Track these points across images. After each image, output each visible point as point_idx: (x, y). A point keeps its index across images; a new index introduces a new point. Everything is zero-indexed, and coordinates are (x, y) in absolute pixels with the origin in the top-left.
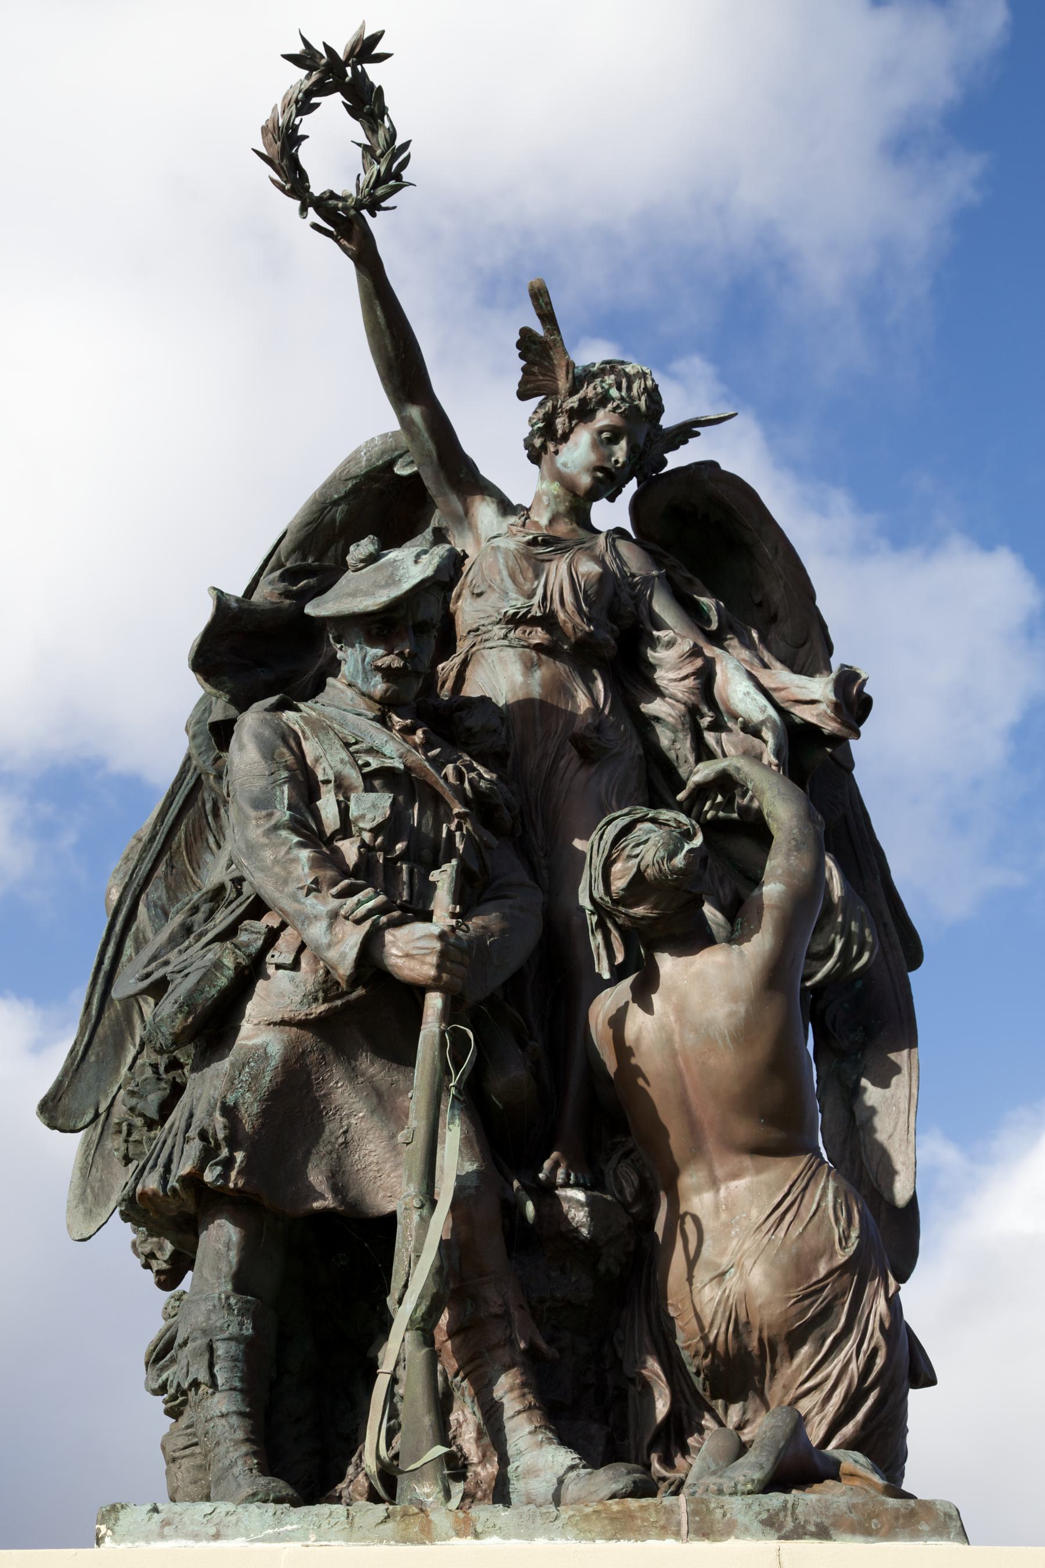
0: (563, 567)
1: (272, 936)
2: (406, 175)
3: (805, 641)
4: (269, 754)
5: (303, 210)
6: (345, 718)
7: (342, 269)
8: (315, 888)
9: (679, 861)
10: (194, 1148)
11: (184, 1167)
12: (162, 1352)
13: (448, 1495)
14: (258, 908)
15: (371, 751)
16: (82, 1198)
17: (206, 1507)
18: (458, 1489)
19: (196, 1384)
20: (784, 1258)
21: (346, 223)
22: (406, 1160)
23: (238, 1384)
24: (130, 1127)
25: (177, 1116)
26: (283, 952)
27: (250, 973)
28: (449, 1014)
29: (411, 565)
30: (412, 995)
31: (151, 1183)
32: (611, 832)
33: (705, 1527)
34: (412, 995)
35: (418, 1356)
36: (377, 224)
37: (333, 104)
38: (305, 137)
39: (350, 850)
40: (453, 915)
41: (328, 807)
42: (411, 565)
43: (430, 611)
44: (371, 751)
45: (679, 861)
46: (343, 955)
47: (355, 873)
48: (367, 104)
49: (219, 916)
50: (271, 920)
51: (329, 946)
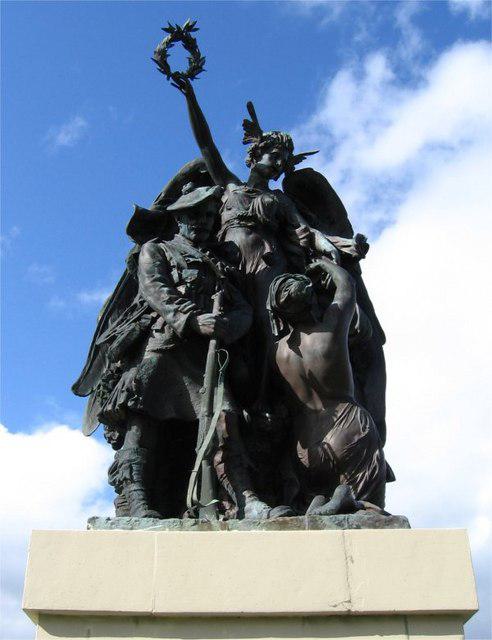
0: (259, 199)
1: (154, 320)
2: (204, 67)
3: (346, 230)
4: (153, 255)
5: (168, 79)
6: (181, 245)
8: (170, 302)
9: (304, 292)
10: (124, 395)
11: (121, 400)
12: (113, 470)
13: (218, 518)
14: (150, 310)
15: (190, 256)
16: (88, 421)
17: (127, 518)
18: (222, 517)
19: (125, 479)
20: (342, 435)
21: (183, 82)
22: (212, 411)
23: (158, 276)
24: (104, 393)
25: (119, 385)
26: (158, 325)
27: (146, 333)
28: (218, 346)
29: (203, 193)
30: (206, 338)
31: (109, 407)
32: (279, 282)
33: (315, 525)
34: (206, 338)
35: (206, 469)
36: (194, 83)
39: (182, 289)
40: (220, 310)
41: (175, 274)
42: (203, 193)
43: (211, 208)
44: (190, 256)
45: (304, 292)
46: (179, 325)
47: (184, 296)
48: (191, 45)
49: (135, 313)
50: (154, 315)
51: (174, 322)
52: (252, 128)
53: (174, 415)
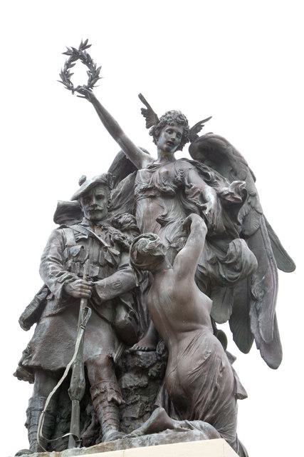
5: (73, 93)
7: (90, 105)
21: (86, 92)
30: (77, 300)
34: (77, 300)
37: (79, 62)
38: (100, 68)
48: (87, 61)
52: (148, 113)
53: (114, 427)
